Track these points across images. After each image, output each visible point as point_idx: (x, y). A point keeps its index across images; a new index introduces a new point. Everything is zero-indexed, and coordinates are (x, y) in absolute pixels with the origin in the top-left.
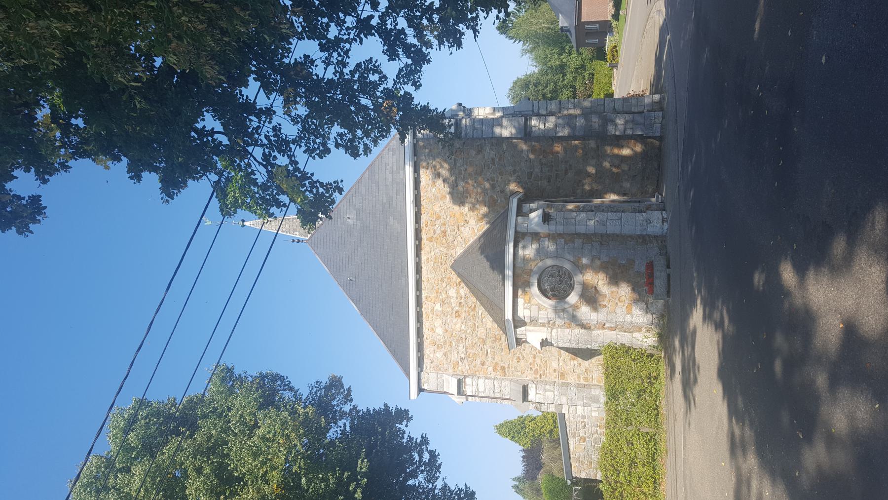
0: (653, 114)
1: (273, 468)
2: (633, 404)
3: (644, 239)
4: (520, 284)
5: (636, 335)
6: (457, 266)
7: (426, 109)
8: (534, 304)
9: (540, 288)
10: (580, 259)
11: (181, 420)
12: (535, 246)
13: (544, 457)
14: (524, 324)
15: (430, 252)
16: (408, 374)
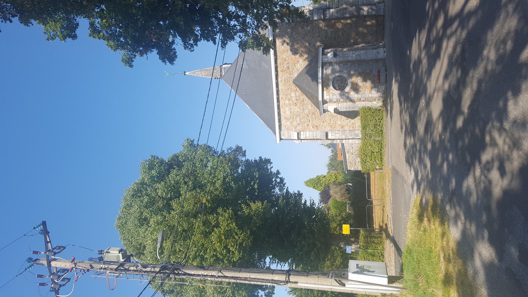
0: (380, 5)
1: (218, 179)
2: (372, 130)
3: (377, 61)
4: (325, 85)
5: (373, 102)
6: (295, 82)
7: (297, 9)
8: (331, 94)
9: (333, 86)
10: (350, 71)
11: (175, 163)
12: (331, 68)
13: (331, 192)
14: (326, 102)
15: (282, 77)
16: (275, 134)
